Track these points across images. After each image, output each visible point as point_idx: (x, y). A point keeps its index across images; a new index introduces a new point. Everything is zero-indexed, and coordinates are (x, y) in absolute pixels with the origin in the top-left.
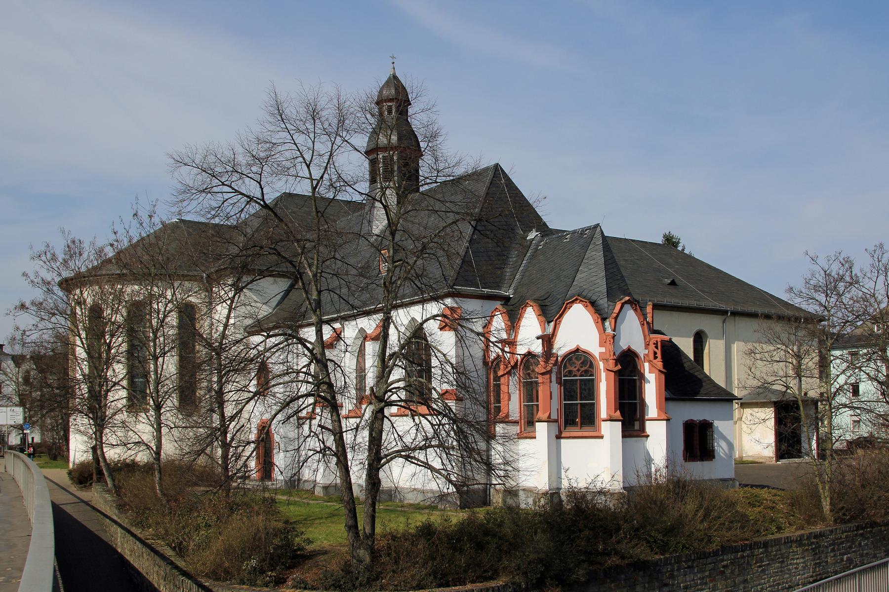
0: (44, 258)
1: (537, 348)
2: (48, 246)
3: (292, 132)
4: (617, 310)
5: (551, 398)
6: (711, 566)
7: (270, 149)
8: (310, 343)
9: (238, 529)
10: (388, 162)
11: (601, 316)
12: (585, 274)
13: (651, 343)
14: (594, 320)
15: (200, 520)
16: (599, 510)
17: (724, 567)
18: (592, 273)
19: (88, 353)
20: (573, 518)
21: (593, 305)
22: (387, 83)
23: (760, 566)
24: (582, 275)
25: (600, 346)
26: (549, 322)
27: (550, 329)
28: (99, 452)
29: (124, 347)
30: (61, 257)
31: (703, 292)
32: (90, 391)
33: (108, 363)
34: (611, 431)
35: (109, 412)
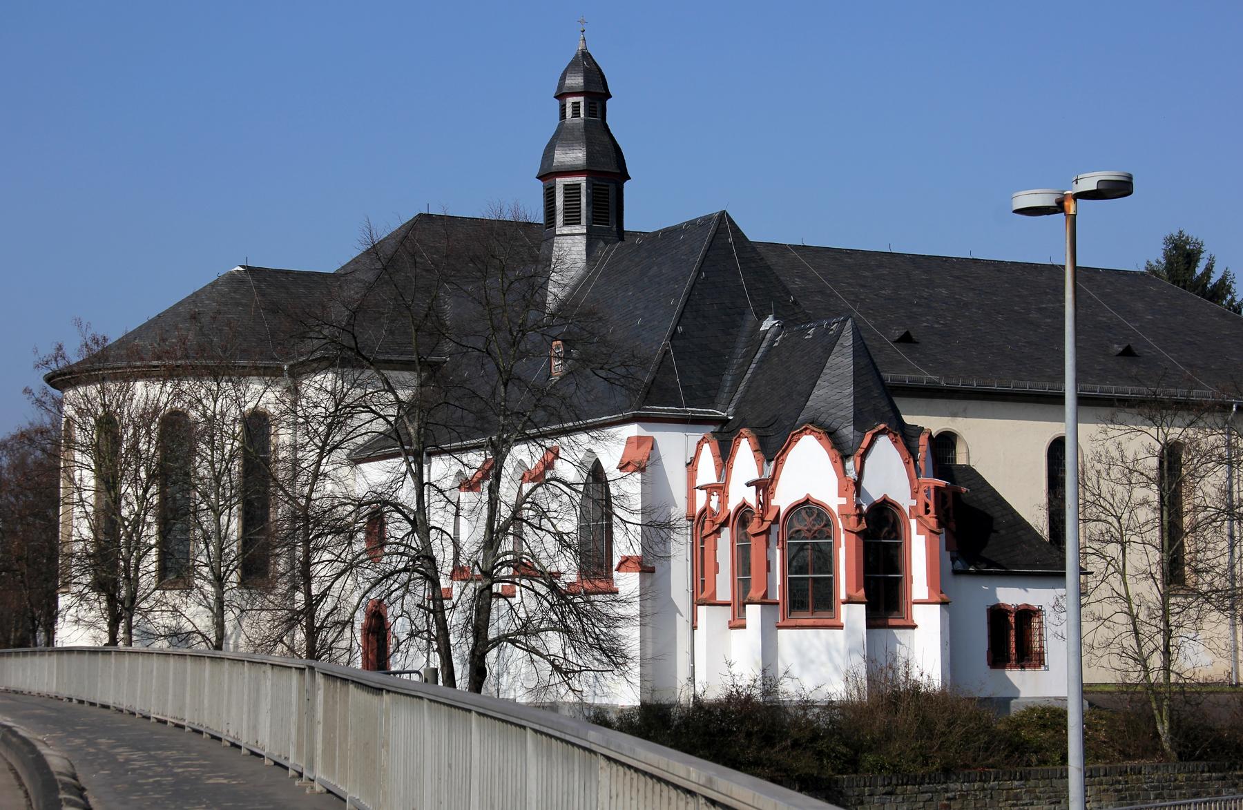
1: (751, 496)
2: (60, 348)
5: (768, 569)
6: (927, 796)
10: (571, 191)
11: (841, 450)
12: (825, 390)
13: (921, 490)
14: (831, 459)
16: (717, 704)
17: (949, 799)
18: (835, 388)
21: (833, 439)
22: (572, 67)
26: (769, 461)
34: (854, 616)
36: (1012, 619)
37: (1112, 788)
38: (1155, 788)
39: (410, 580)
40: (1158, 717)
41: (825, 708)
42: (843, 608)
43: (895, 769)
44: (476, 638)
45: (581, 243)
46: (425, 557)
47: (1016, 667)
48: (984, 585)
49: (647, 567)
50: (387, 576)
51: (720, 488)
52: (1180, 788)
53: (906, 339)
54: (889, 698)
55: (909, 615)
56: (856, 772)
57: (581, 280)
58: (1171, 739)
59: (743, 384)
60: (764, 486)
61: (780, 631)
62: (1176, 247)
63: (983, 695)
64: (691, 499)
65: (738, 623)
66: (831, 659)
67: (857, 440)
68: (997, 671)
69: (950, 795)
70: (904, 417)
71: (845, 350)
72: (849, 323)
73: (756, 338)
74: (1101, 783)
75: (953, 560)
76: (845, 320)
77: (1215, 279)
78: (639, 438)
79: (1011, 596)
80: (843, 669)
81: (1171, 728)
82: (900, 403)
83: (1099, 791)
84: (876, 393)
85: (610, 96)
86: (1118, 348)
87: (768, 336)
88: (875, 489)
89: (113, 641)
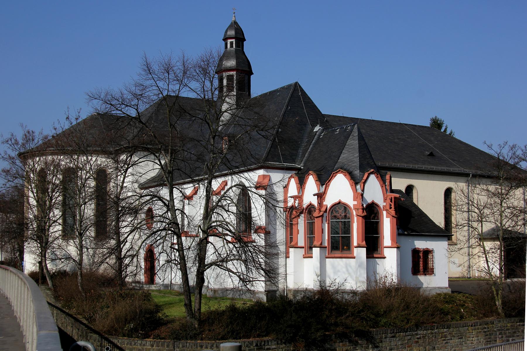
0: (10, 142)
1: (315, 201)
2: (12, 135)
3: (156, 79)
4: (365, 178)
5: (322, 233)
6: (409, 337)
7: (143, 90)
8: (166, 200)
9: (122, 308)
11: (355, 180)
12: (346, 155)
13: (388, 198)
14: (350, 184)
15: (103, 304)
17: (418, 338)
18: (351, 153)
19: (37, 202)
20: (322, 303)
22: (230, 27)
23: (444, 340)
24: (344, 156)
25: (354, 200)
26: (322, 185)
27: (322, 189)
28: (43, 264)
29: (60, 198)
30: (21, 141)
31: (454, 160)
32: (38, 226)
33: (51, 208)
34: (361, 253)
35: (50, 239)
36: (421, 255)
37: (482, 331)
38: (499, 330)
39: (166, 235)
40: (496, 298)
44: (200, 264)
46: (174, 223)
47: (423, 274)
50: (155, 233)
51: (299, 197)
52: (508, 330)
58: (503, 308)
59: (307, 154)
60: (321, 196)
61: (327, 259)
62: (434, 122)
66: (347, 270)
68: (415, 276)
69: (418, 336)
72: (356, 126)
73: (312, 135)
74: (478, 329)
75: (398, 229)
76: (354, 125)
77: (448, 133)
78: (264, 175)
79: (421, 244)
81: (502, 303)
83: (477, 332)
86: (428, 153)
87: (318, 133)
88: (369, 198)
89: (392, 191)
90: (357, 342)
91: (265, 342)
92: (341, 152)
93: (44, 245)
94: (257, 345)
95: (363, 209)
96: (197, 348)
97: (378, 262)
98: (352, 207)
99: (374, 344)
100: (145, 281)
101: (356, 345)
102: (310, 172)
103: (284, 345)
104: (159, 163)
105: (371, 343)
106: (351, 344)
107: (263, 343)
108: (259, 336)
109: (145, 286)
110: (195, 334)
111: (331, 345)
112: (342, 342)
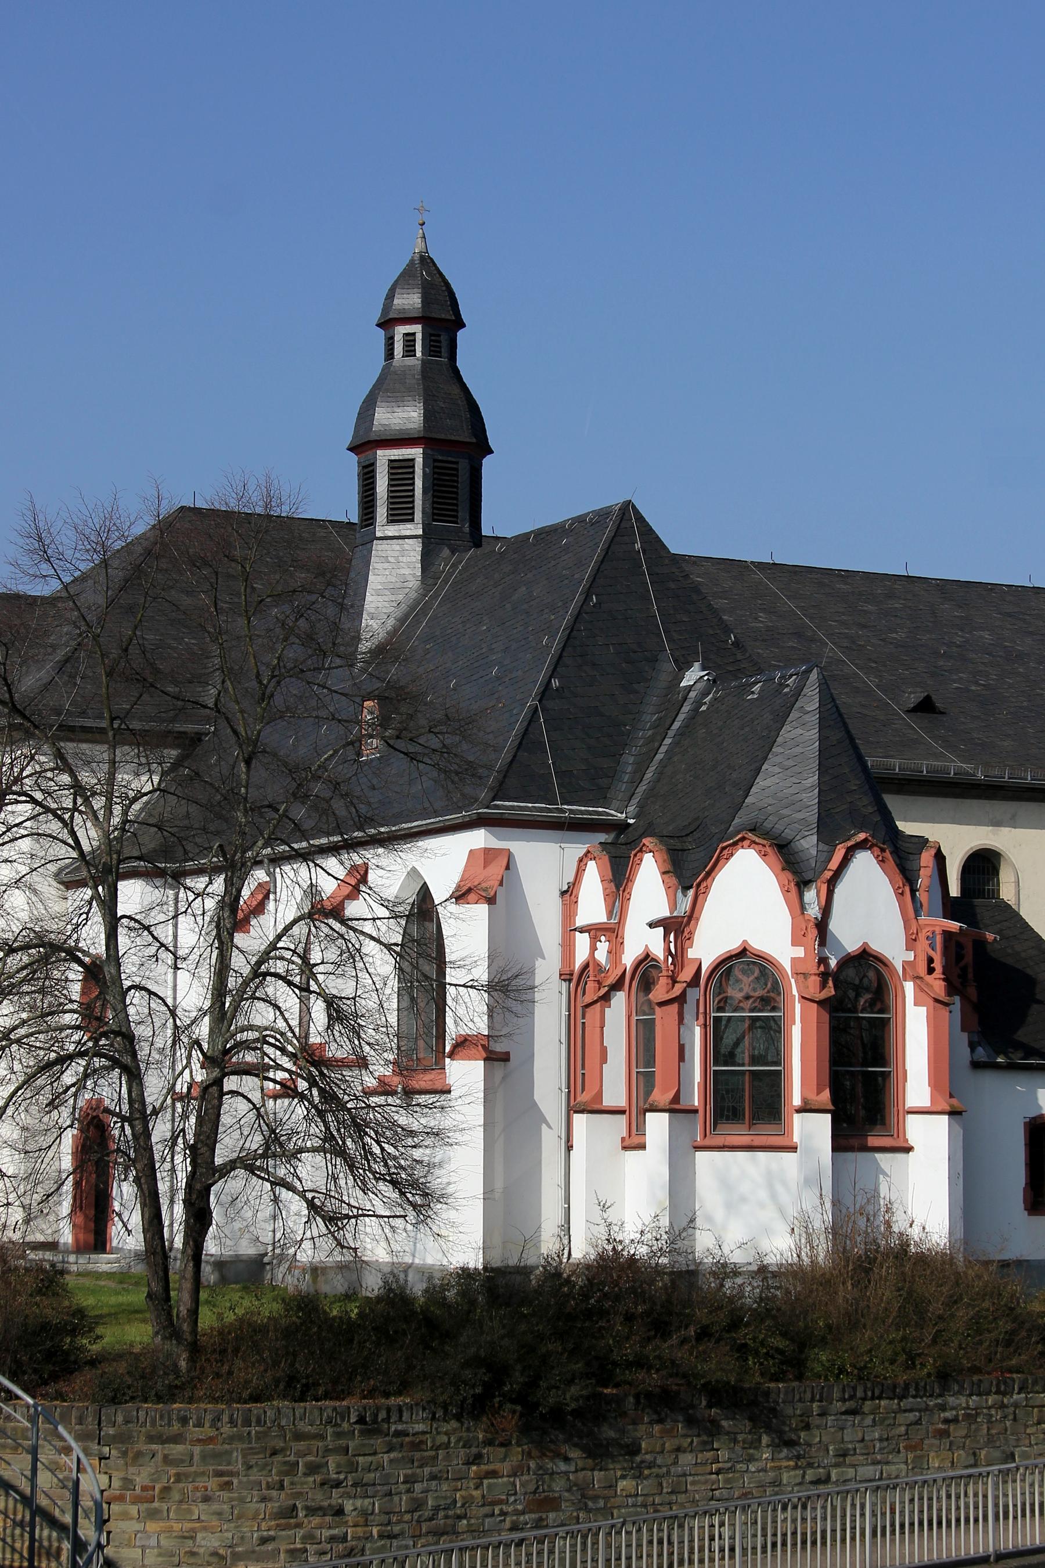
1: (656, 943)
4: (834, 864)
5: (682, 1057)
6: (912, 1416)
10: (401, 470)
11: (797, 873)
13: (922, 936)
17: (946, 1421)
18: (789, 778)
24: (768, 782)
26: (686, 888)
34: (814, 1131)
41: (753, 1275)
42: (797, 1118)
43: (862, 1374)
45: (414, 550)
48: (1017, 1085)
49: (497, 1055)
51: (611, 932)
53: (926, 706)
54: (866, 1258)
55: (901, 1131)
56: (800, 1377)
57: (412, 608)
59: (652, 769)
60: (678, 927)
63: (1007, 1256)
64: (568, 948)
65: (636, 1140)
66: (774, 1196)
67: (823, 857)
69: (948, 1415)
70: (897, 823)
71: (806, 718)
72: (814, 675)
75: (972, 1046)
76: (808, 671)
80: (792, 1211)
82: (892, 802)
84: (854, 784)
85: (463, 325)
88: (849, 933)
90: (714, 1422)
91: (389, 1410)
92: (758, 771)
93: (339, 806)
94: (361, 1420)
95: (825, 976)
96: (169, 1424)
97: (883, 1165)
98: (788, 967)
99: (780, 1433)
100: (76, 1240)
101: (711, 1435)
102: (646, 841)
103: (454, 1424)
104: (71, 841)
105: (769, 1429)
106: (695, 1431)
107: (382, 1415)
108: (371, 1394)
109: (72, 1258)
110: (171, 1387)
111: (623, 1432)
112: (660, 1421)
